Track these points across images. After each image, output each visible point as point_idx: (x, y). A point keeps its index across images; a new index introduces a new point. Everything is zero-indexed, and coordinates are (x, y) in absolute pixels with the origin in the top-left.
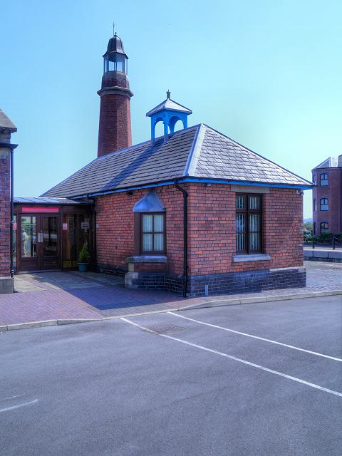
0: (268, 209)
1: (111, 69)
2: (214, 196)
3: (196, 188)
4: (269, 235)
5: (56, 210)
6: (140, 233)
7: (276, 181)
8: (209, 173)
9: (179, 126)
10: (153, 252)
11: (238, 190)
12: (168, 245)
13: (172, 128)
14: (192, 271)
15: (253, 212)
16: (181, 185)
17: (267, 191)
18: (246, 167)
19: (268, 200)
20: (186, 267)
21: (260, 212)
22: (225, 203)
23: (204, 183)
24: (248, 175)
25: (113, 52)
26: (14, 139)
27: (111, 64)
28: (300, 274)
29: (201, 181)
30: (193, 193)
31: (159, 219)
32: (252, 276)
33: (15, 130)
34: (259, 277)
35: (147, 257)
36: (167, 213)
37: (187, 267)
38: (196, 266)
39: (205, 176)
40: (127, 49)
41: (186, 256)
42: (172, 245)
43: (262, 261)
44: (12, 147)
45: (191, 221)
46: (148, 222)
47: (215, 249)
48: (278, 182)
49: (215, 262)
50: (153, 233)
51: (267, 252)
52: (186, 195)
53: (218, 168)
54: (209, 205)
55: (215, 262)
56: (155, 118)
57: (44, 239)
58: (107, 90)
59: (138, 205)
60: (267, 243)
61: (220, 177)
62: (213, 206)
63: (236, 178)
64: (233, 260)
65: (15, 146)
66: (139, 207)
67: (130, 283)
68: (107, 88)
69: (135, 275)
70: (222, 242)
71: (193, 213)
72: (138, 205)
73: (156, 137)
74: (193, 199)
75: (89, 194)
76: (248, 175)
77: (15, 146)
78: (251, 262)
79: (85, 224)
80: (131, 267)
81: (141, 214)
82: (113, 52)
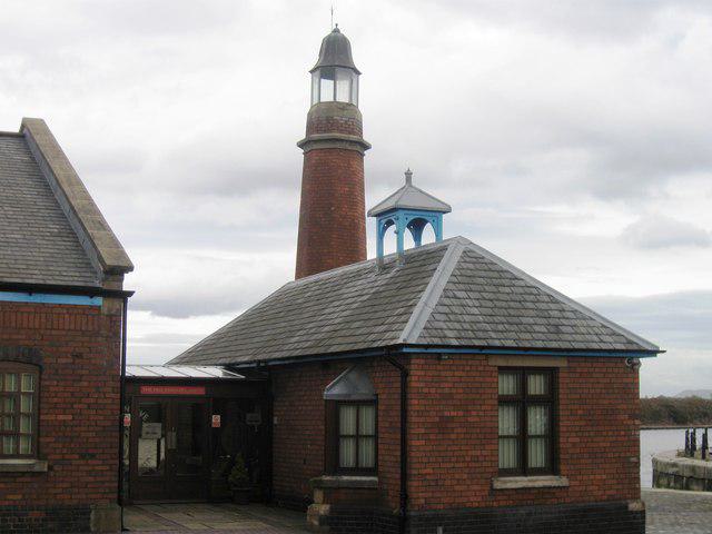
0: (563, 394)
1: (327, 97)
2: (456, 373)
3: (422, 361)
4: (567, 441)
5: (200, 391)
6: (334, 436)
7: (577, 346)
8: (445, 337)
9: (428, 236)
10: (357, 470)
11: (502, 363)
12: (380, 458)
13: (417, 238)
14: (413, 502)
15: (537, 401)
16: (396, 357)
17: (561, 363)
18: (524, 320)
19: (564, 380)
20: (405, 497)
21: (549, 401)
22: (478, 385)
23: (433, 353)
24: (523, 336)
25: (335, 58)
26: (128, 282)
27: (327, 84)
28: (632, 512)
29: (429, 351)
30: (416, 371)
31: (368, 415)
32: (529, 514)
33: (130, 268)
34: (544, 516)
35: (345, 478)
36: (380, 402)
37: (407, 497)
38: (419, 496)
39: (437, 341)
40: (358, 58)
41: (404, 477)
42: (387, 458)
43: (550, 488)
44: (124, 296)
45: (413, 418)
46: (348, 419)
47: (457, 465)
48: (583, 346)
49: (457, 488)
50: (357, 437)
51: (562, 472)
52: (405, 374)
53: (466, 326)
54: (447, 391)
55: (457, 488)
56: (384, 221)
57: (323, 503)
58: (316, 141)
59: (331, 387)
60: (562, 456)
61: (463, 343)
62: (454, 391)
63: (497, 343)
64: (492, 485)
65: (130, 294)
66: (335, 390)
67: (316, 523)
68: (316, 136)
69: (323, 509)
70: (474, 453)
71: (415, 404)
72: (331, 387)
73: (405, 249)
74: (415, 381)
75: (260, 361)
76: (523, 336)
77: (130, 294)
78: (530, 489)
79: (253, 418)
80: (318, 495)
81: (336, 406)
82: (335, 58)
